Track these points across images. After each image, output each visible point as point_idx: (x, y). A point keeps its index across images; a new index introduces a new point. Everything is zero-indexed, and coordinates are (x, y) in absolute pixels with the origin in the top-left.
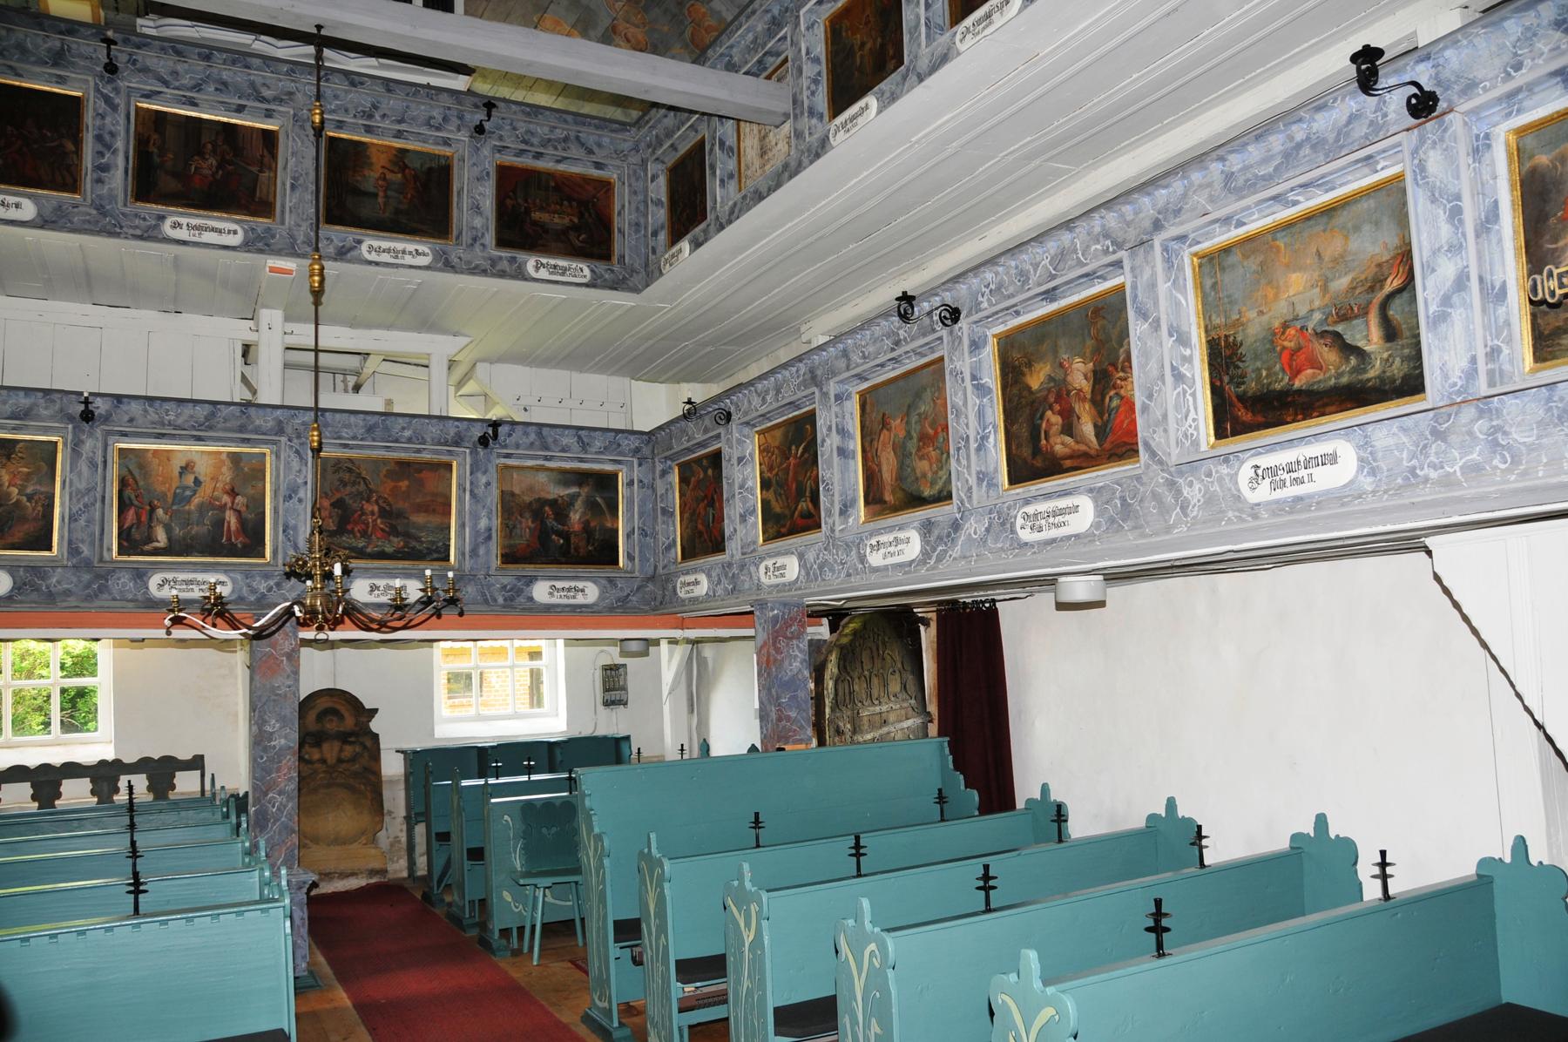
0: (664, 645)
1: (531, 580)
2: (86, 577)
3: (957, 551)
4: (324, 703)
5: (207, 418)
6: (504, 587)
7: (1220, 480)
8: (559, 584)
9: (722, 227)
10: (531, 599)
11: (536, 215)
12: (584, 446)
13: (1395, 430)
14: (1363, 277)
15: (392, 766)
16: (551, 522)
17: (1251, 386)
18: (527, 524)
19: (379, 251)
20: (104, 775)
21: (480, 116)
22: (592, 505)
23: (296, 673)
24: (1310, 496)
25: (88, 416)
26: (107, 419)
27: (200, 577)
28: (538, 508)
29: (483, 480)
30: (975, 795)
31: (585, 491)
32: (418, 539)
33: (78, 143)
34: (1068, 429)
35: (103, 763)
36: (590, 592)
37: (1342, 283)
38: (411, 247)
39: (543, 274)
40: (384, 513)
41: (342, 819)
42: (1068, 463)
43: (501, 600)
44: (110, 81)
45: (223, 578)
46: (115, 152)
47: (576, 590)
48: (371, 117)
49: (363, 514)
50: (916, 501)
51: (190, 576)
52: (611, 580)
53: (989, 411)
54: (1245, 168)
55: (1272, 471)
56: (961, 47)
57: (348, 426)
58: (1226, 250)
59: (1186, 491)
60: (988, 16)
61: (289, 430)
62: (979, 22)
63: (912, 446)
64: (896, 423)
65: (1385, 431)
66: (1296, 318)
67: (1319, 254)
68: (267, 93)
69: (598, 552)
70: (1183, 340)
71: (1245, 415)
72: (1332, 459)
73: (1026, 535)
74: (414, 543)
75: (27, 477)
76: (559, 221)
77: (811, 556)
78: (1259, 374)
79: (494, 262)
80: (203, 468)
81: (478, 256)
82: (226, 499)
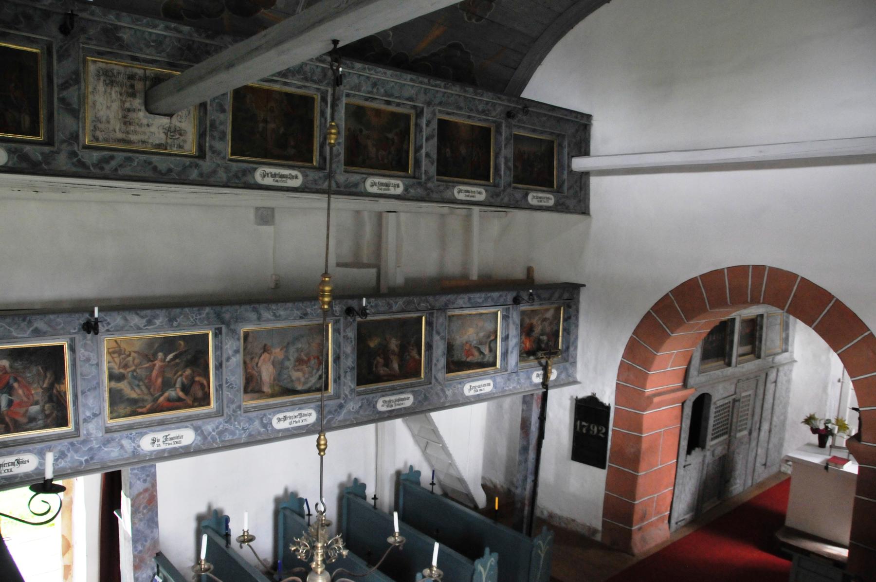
37: (482, 334)
42: (385, 378)
55: (475, 387)
59: (447, 392)
71: (452, 367)
78: (460, 356)
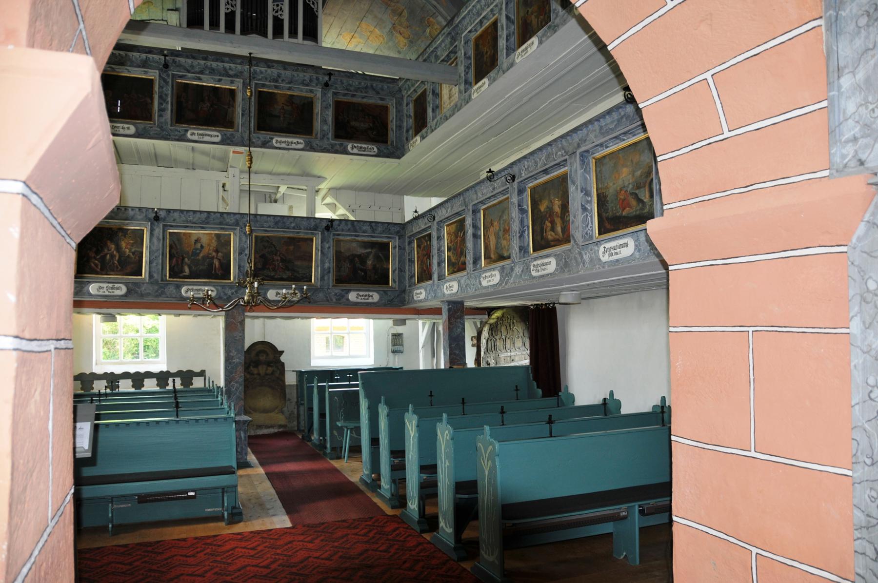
1: (349, 291)
2: (156, 287)
3: (512, 280)
4: (259, 348)
5: (206, 219)
6: (336, 294)
8: (361, 293)
9: (433, 131)
10: (348, 300)
11: (353, 123)
12: (373, 231)
15: (291, 379)
16: (358, 265)
17: (610, 214)
18: (347, 266)
19: (281, 142)
20: (162, 377)
21: (327, 78)
22: (377, 257)
23: (244, 330)
24: (621, 259)
25: (157, 218)
26: (164, 220)
27: (203, 288)
28: (352, 259)
29: (327, 246)
30: (540, 391)
31: (374, 251)
32: (329, 268)
33: (152, 99)
34: (553, 229)
35: (162, 372)
36: (375, 297)
37: (638, 173)
38: (295, 140)
39: (355, 151)
40: (282, 260)
41: (266, 401)
42: (552, 243)
43: (334, 300)
44: (165, 72)
45: (213, 288)
46: (167, 103)
47: (369, 296)
48: (277, 81)
49: (273, 260)
50: (502, 258)
51: (199, 287)
52: (385, 292)
53: (525, 220)
54: (606, 125)
56: (517, 61)
57: (267, 222)
58: (604, 157)
60: (526, 49)
61: (241, 224)
62: (523, 51)
63: (501, 233)
64: (495, 224)
68: (231, 73)
69: (380, 278)
70: (587, 193)
72: (626, 245)
73: (534, 273)
74: (295, 274)
75: (132, 245)
76: (363, 126)
77: (462, 281)
78: (613, 209)
79: (333, 146)
80: (204, 241)
81: (325, 144)
82: (214, 254)
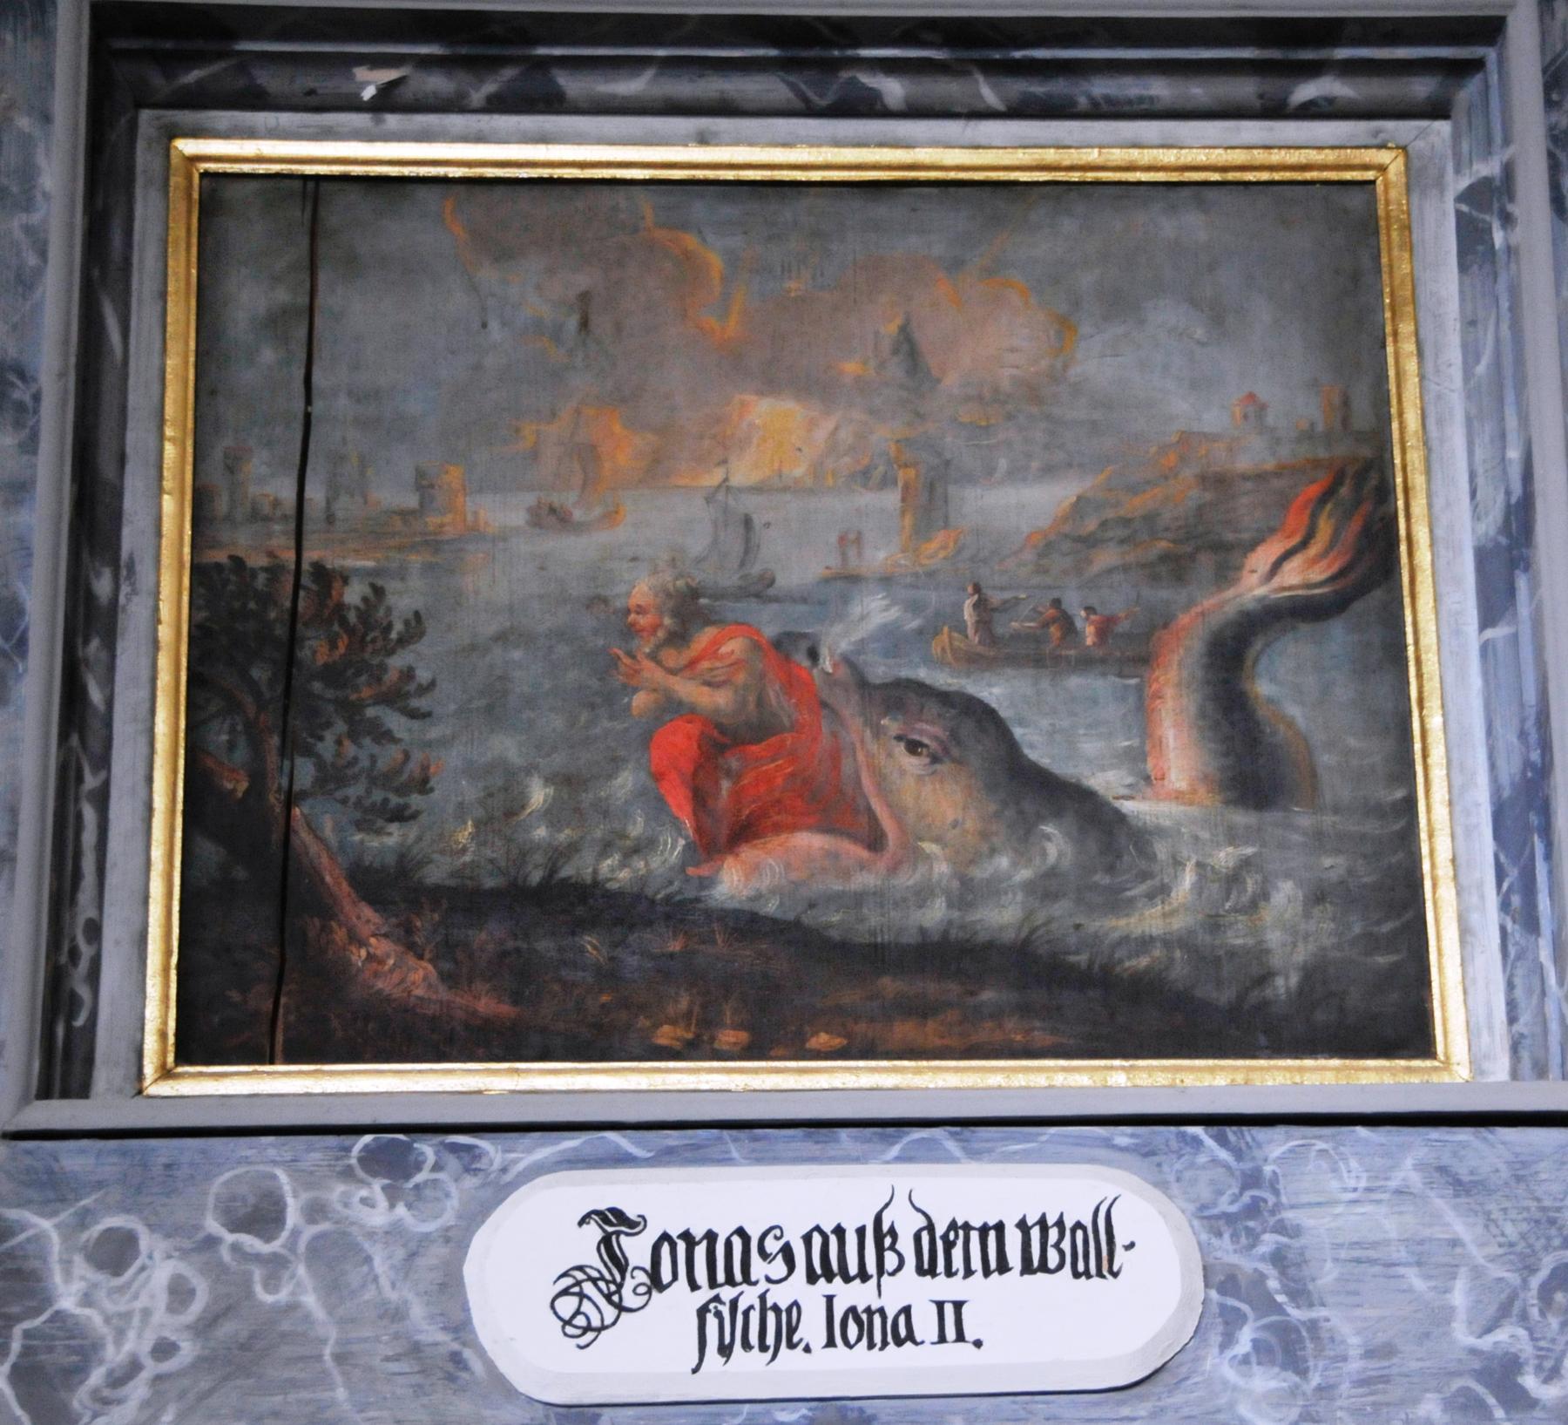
0: (1514, 1278)
7: (336, 1254)
13: (1407, 1172)
14: (1136, 506)
55: (722, 1258)
65: (1354, 1174)
66: (761, 590)
67: (908, 348)
72: (1092, 1250)
